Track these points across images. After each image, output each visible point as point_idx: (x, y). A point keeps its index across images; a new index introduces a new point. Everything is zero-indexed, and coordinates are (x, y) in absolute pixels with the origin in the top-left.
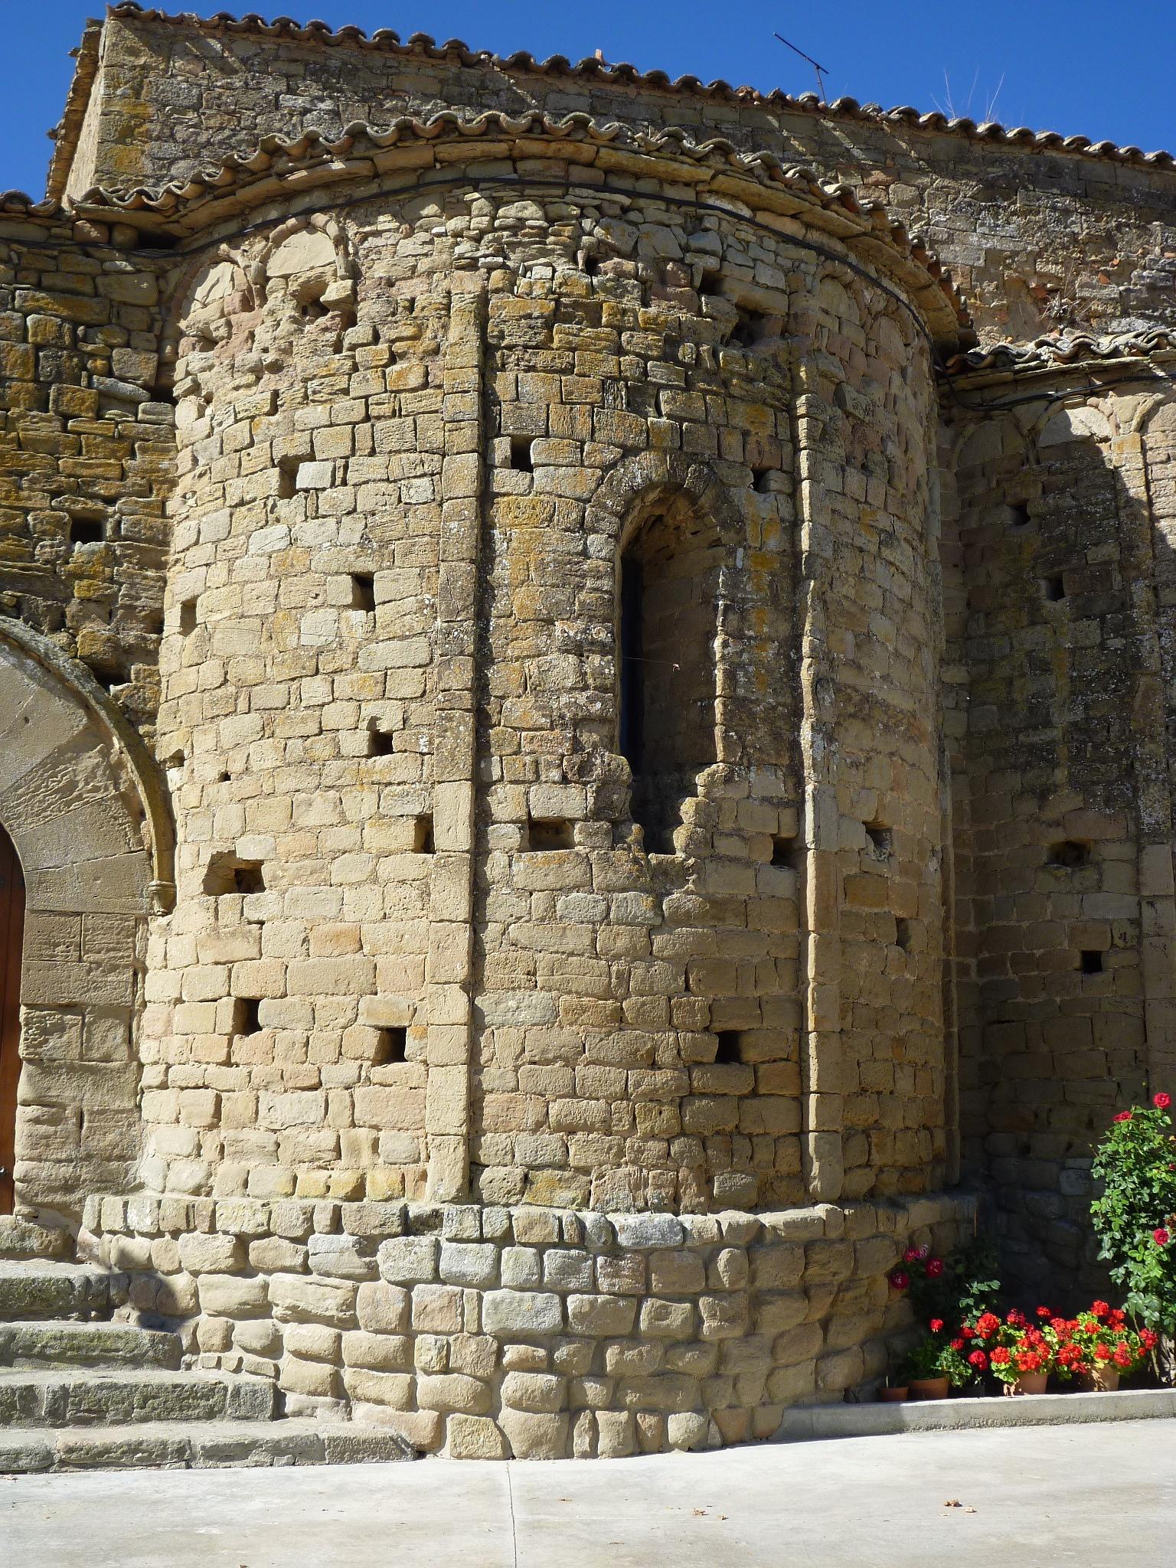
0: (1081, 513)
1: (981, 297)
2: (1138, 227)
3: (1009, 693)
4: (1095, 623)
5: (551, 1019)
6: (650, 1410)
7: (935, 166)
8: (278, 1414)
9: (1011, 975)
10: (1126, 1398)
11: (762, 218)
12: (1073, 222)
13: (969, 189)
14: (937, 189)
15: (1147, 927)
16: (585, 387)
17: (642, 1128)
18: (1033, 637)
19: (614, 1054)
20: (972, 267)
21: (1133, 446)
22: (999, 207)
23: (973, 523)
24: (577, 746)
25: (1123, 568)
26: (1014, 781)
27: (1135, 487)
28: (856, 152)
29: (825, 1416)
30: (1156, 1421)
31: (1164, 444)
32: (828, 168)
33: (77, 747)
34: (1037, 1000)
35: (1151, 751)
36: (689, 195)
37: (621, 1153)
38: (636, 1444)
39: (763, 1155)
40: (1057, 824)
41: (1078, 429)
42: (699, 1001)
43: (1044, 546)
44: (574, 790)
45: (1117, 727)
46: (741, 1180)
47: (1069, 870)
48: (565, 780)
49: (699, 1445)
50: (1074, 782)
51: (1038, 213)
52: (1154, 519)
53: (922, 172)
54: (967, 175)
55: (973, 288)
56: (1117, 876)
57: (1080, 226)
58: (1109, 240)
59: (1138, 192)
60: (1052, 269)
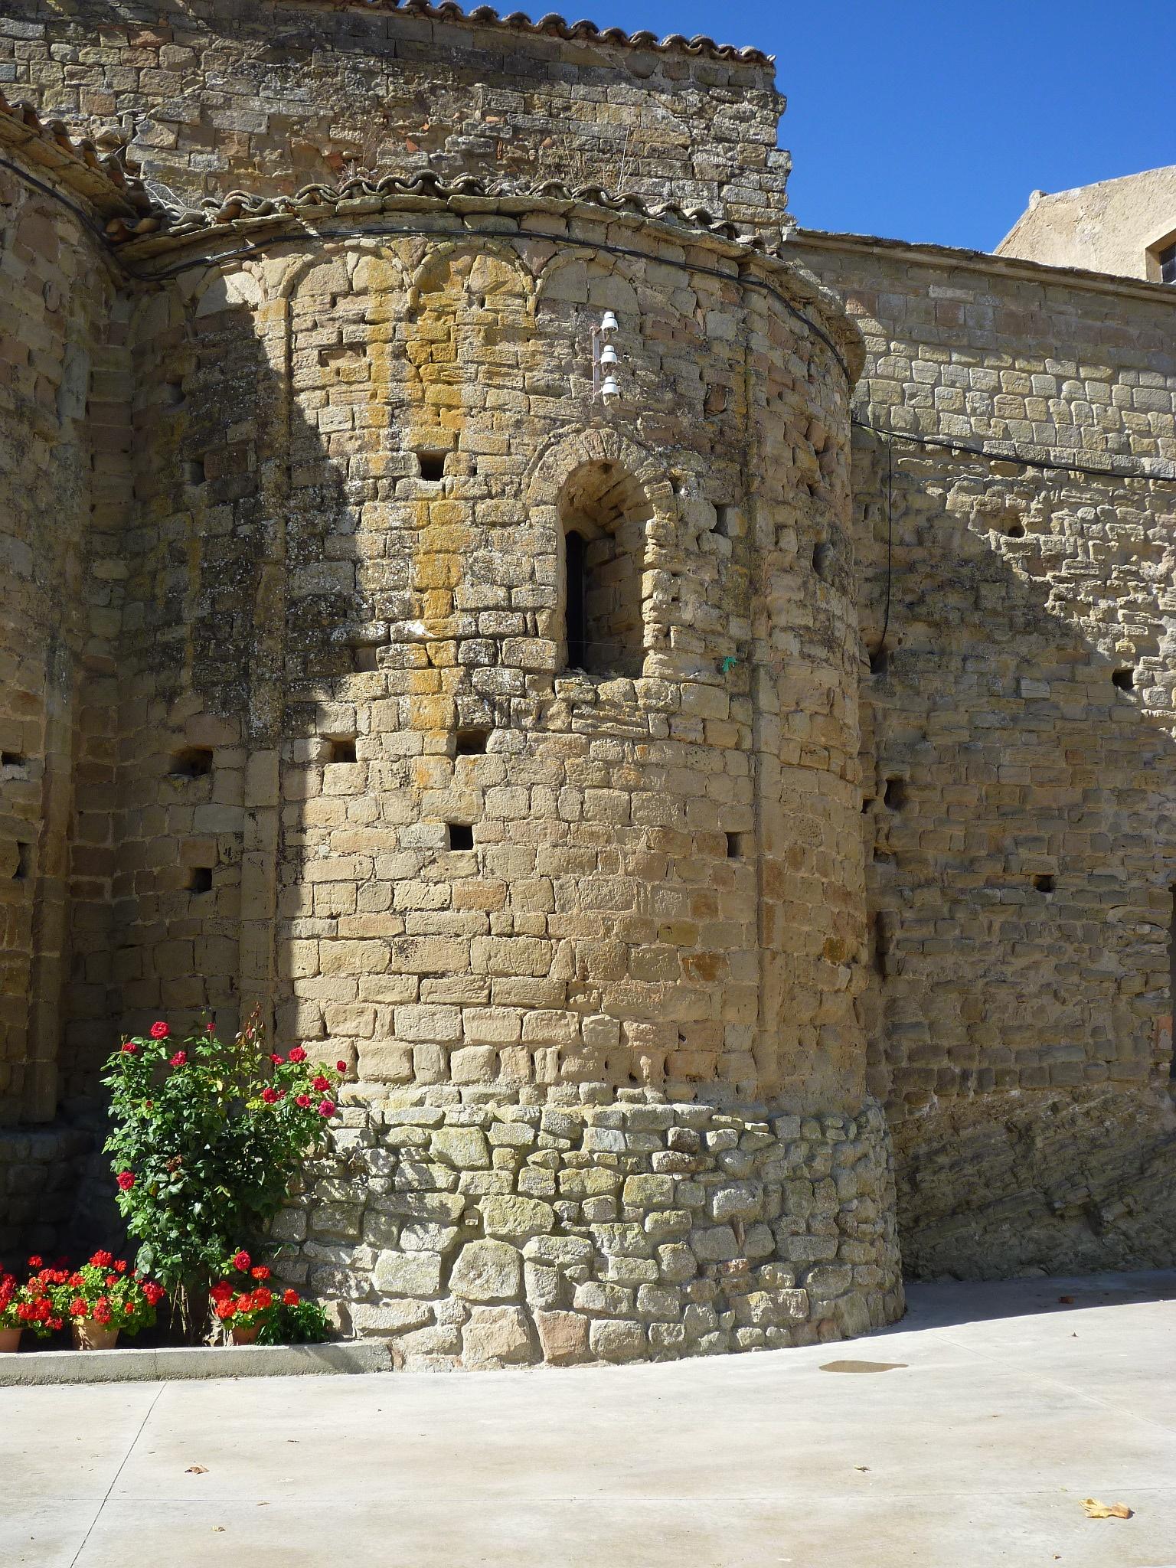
0: (227, 388)
1: (261, 166)
2: (457, 90)
3: (153, 587)
4: (228, 509)
9: (135, 896)
10: (95, 1358)
12: (378, 85)
13: (254, 49)
14: (216, 50)
15: (248, 842)
18: (175, 525)
20: (252, 133)
21: (277, 313)
22: (289, 69)
23: (141, 405)
25: (258, 449)
26: (149, 683)
27: (276, 359)
28: (123, 11)
30: (132, 1384)
31: (310, 310)
32: (88, 28)
34: (151, 922)
35: (270, 647)
40: (180, 729)
41: (233, 298)
43: (191, 426)
45: (239, 622)
47: (186, 779)
50: (203, 688)
51: (336, 75)
52: (293, 392)
53: (200, 32)
54: (254, 34)
55: (251, 156)
56: (224, 782)
57: (384, 89)
58: (421, 103)
59: (458, 50)
60: (348, 135)
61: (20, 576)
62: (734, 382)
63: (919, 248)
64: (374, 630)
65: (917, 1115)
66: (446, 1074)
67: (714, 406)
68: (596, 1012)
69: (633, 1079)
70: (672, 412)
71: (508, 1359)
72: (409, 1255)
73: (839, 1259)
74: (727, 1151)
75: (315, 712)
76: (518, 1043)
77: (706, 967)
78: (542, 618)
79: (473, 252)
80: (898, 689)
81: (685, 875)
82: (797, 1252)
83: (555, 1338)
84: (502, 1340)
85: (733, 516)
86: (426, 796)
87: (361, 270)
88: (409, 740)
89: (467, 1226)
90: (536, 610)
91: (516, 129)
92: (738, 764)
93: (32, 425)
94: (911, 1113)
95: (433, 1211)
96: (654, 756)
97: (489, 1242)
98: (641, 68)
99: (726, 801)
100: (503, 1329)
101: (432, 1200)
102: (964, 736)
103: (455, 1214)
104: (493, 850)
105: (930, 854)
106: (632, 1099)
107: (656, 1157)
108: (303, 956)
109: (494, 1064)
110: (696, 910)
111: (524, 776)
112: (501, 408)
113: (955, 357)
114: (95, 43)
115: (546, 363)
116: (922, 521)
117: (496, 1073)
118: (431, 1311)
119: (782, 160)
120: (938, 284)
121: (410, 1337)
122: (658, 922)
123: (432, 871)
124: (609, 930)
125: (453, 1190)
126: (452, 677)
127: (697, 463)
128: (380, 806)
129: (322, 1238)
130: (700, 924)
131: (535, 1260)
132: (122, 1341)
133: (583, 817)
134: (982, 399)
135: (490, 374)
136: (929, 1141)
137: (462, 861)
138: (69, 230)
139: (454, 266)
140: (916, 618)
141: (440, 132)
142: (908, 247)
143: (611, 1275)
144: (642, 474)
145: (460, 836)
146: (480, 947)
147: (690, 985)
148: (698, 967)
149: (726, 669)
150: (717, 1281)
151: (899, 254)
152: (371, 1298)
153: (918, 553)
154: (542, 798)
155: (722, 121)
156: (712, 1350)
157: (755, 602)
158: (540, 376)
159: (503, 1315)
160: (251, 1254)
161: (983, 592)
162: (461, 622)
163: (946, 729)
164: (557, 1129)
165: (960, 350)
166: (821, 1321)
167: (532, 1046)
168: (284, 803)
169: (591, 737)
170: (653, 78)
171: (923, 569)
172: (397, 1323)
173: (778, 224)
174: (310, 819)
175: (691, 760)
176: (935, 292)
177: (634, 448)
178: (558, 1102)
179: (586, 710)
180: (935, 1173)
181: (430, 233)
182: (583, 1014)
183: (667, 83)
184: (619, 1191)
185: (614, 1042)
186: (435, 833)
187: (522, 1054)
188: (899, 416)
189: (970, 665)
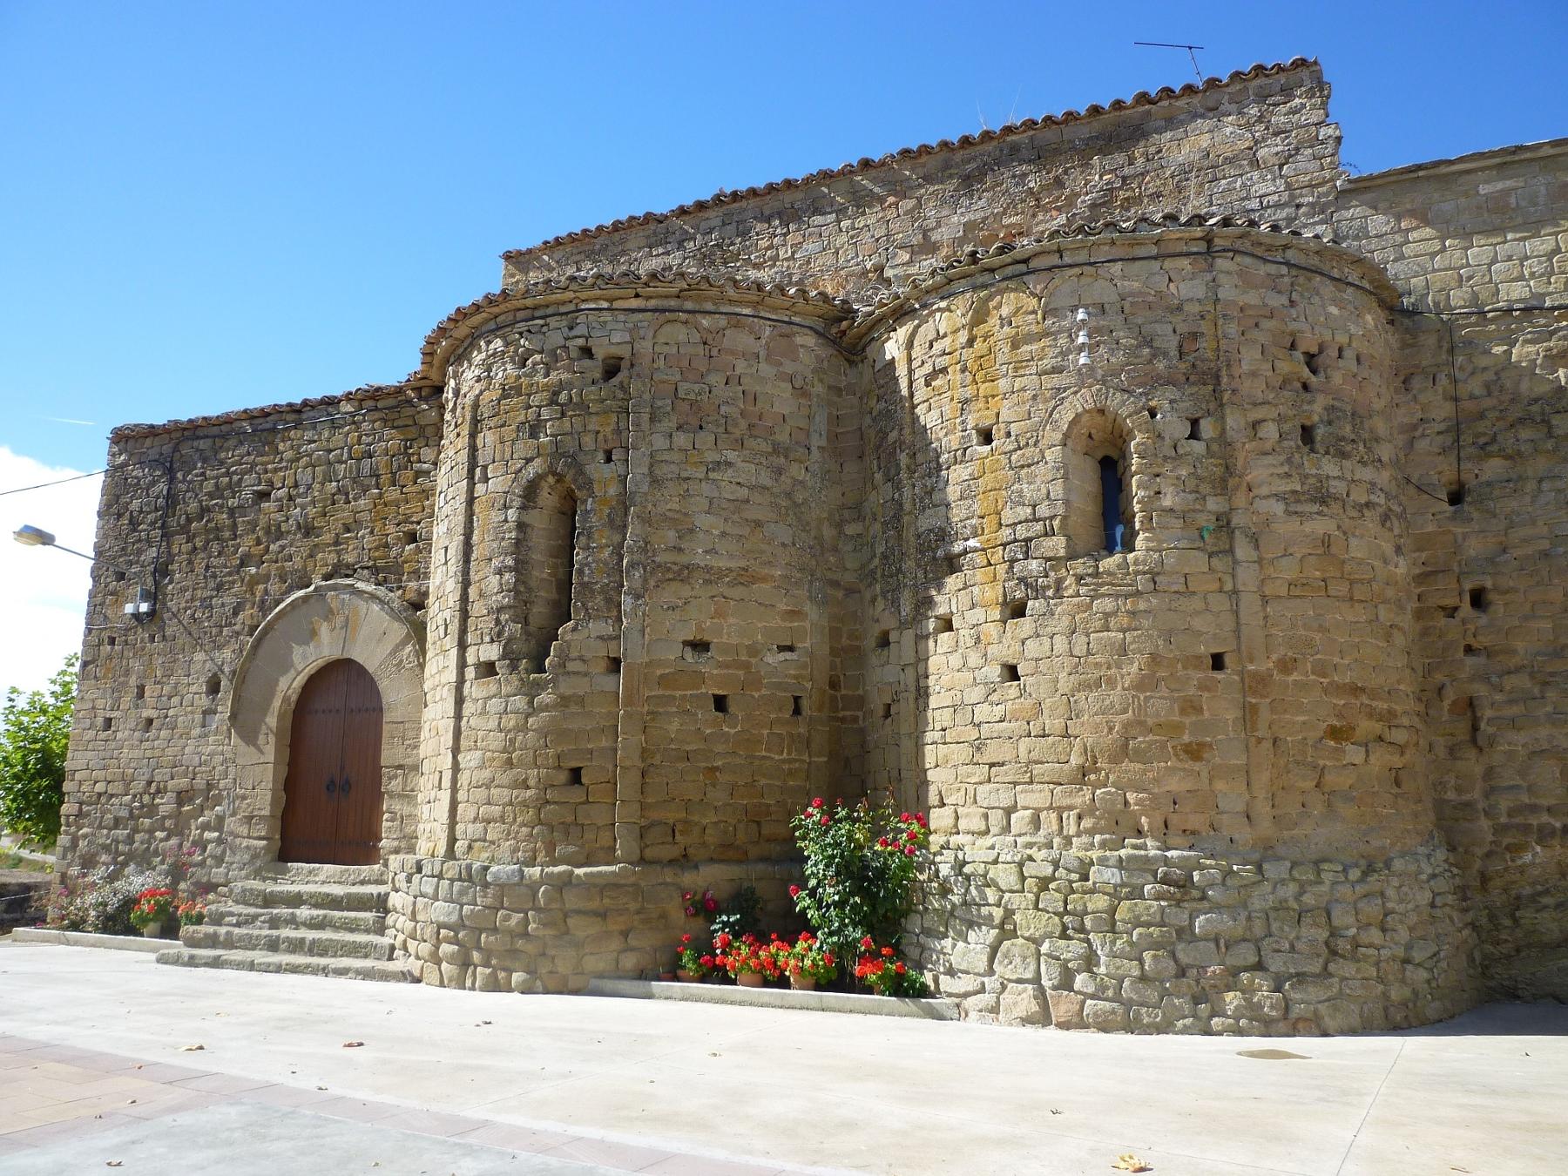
5: (481, 767)
6: (504, 969)
7: (928, 179)
8: (390, 958)
11: (616, 304)
16: (508, 432)
17: (519, 820)
19: (506, 782)
24: (498, 622)
28: (876, 190)
29: (624, 985)
32: (858, 207)
33: (404, 643)
36: (572, 307)
37: (509, 834)
38: (493, 986)
39: (589, 836)
42: (551, 752)
44: (495, 645)
46: (572, 849)
48: (492, 641)
49: (527, 990)
53: (920, 186)
54: (951, 177)
58: (1059, 183)
60: (1013, 220)
61: (783, 545)
62: (1205, 327)
63: (1461, 160)
64: (957, 548)
65: (1519, 862)
66: (1007, 829)
67: (1186, 349)
68: (1105, 786)
69: (1139, 833)
70: (1150, 362)
71: (1027, 1021)
72: (972, 946)
73: (1326, 973)
74: (1211, 886)
75: (929, 602)
76: (1051, 808)
77: (1194, 752)
78: (1056, 523)
79: (1001, 292)
80: (1475, 515)
81: (1173, 686)
82: (1276, 964)
83: (1063, 1006)
84: (1023, 1007)
85: (1207, 428)
86: (989, 649)
87: (943, 322)
88: (978, 615)
89: (1007, 930)
90: (1052, 518)
91: (1124, 179)
92: (1220, 603)
93: (786, 457)
94: (1513, 860)
95: (985, 918)
96: (1142, 606)
97: (1021, 941)
98: (1211, 104)
99: (1210, 633)
100: (1022, 1000)
101: (984, 911)
102: (1545, 544)
103: (997, 921)
104: (1030, 680)
105: (1520, 645)
106: (1135, 847)
107: (1147, 888)
108: (930, 755)
109: (1036, 823)
110: (1183, 712)
111: (1049, 629)
112: (1023, 389)
113: (1509, 236)
114: (864, 213)
115: (1051, 352)
116: (1490, 376)
117: (1038, 828)
118: (983, 984)
119: (1330, 131)
120: (1487, 182)
121: (971, 1000)
122: (1150, 722)
123: (994, 697)
124: (1111, 729)
125: (999, 905)
126: (1002, 569)
127: (1171, 392)
128: (964, 657)
129: (928, 932)
130: (1187, 721)
131: (1049, 956)
132: (818, 987)
133: (1089, 653)
134: (1540, 263)
135: (1016, 369)
136: (1533, 884)
137: (1012, 689)
138: (810, 340)
139: (992, 304)
140: (1490, 455)
141: (1071, 201)
142: (1451, 162)
143: (1103, 970)
144: (1124, 412)
145: (1012, 673)
146: (1025, 744)
147: (1179, 765)
148: (1186, 752)
149: (1206, 535)
150: (1198, 982)
151: (1444, 170)
152: (951, 972)
153: (1488, 403)
154: (1060, 643)
155: (1279, 119)
156: (1185, 1031)
157: (1232, 482)
158: (1047, 363)
159: (1025, 990)
160: (880, 942)
161: (1554, 422)
162: (1005, 534)
163: (1526, 541)
164: (1070, 866)
165: (1514, 229)
166: (1298, 1020)
167: (1060, 811)
168: (918, 660)
169: (1093, 598)
170: (1222, 108)
171: (1491, 415)
172: (963, 990)
173: (1332, 180)
174: (931, 670)
175: (1174, 604)
176: (1484, 189)
177: (1118, 394)
178: (1079, 849)
179: (1089, 580)
180: (1538, 911)
181: (975, 288)
182: (1095, 787)
183: (1234, 107)
184: (1112, 911)
185: (1120, 806)
186: (994, 672)
187: (1054, 816)
188: (1458, 298)
189: (1546, 486)
